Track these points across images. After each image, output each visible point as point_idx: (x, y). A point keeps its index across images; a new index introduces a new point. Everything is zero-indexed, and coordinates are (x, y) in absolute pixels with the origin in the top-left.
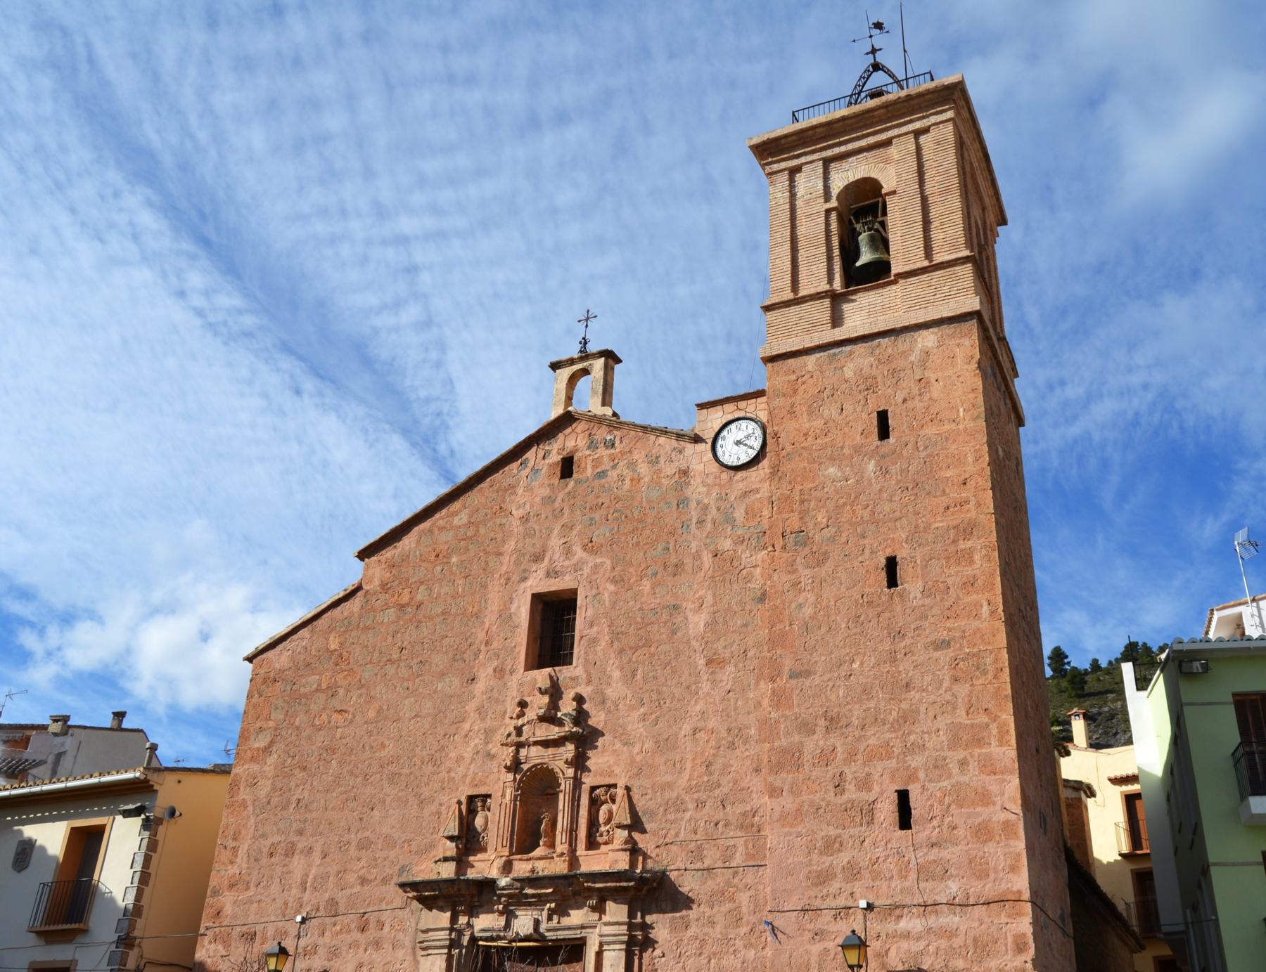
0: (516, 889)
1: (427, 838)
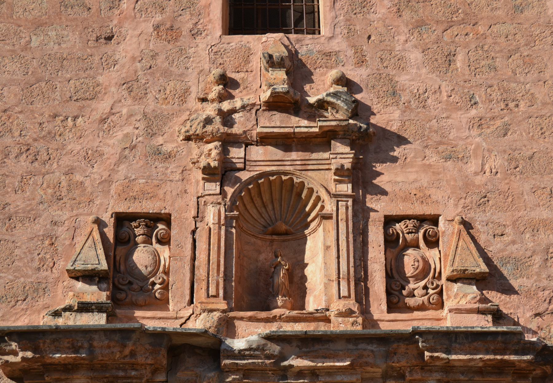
0: (268, 357)
1: (26, 276)
